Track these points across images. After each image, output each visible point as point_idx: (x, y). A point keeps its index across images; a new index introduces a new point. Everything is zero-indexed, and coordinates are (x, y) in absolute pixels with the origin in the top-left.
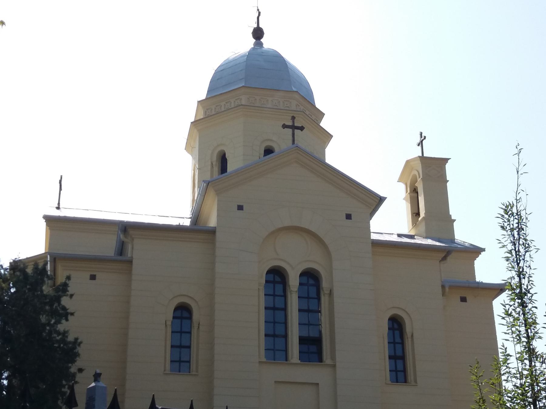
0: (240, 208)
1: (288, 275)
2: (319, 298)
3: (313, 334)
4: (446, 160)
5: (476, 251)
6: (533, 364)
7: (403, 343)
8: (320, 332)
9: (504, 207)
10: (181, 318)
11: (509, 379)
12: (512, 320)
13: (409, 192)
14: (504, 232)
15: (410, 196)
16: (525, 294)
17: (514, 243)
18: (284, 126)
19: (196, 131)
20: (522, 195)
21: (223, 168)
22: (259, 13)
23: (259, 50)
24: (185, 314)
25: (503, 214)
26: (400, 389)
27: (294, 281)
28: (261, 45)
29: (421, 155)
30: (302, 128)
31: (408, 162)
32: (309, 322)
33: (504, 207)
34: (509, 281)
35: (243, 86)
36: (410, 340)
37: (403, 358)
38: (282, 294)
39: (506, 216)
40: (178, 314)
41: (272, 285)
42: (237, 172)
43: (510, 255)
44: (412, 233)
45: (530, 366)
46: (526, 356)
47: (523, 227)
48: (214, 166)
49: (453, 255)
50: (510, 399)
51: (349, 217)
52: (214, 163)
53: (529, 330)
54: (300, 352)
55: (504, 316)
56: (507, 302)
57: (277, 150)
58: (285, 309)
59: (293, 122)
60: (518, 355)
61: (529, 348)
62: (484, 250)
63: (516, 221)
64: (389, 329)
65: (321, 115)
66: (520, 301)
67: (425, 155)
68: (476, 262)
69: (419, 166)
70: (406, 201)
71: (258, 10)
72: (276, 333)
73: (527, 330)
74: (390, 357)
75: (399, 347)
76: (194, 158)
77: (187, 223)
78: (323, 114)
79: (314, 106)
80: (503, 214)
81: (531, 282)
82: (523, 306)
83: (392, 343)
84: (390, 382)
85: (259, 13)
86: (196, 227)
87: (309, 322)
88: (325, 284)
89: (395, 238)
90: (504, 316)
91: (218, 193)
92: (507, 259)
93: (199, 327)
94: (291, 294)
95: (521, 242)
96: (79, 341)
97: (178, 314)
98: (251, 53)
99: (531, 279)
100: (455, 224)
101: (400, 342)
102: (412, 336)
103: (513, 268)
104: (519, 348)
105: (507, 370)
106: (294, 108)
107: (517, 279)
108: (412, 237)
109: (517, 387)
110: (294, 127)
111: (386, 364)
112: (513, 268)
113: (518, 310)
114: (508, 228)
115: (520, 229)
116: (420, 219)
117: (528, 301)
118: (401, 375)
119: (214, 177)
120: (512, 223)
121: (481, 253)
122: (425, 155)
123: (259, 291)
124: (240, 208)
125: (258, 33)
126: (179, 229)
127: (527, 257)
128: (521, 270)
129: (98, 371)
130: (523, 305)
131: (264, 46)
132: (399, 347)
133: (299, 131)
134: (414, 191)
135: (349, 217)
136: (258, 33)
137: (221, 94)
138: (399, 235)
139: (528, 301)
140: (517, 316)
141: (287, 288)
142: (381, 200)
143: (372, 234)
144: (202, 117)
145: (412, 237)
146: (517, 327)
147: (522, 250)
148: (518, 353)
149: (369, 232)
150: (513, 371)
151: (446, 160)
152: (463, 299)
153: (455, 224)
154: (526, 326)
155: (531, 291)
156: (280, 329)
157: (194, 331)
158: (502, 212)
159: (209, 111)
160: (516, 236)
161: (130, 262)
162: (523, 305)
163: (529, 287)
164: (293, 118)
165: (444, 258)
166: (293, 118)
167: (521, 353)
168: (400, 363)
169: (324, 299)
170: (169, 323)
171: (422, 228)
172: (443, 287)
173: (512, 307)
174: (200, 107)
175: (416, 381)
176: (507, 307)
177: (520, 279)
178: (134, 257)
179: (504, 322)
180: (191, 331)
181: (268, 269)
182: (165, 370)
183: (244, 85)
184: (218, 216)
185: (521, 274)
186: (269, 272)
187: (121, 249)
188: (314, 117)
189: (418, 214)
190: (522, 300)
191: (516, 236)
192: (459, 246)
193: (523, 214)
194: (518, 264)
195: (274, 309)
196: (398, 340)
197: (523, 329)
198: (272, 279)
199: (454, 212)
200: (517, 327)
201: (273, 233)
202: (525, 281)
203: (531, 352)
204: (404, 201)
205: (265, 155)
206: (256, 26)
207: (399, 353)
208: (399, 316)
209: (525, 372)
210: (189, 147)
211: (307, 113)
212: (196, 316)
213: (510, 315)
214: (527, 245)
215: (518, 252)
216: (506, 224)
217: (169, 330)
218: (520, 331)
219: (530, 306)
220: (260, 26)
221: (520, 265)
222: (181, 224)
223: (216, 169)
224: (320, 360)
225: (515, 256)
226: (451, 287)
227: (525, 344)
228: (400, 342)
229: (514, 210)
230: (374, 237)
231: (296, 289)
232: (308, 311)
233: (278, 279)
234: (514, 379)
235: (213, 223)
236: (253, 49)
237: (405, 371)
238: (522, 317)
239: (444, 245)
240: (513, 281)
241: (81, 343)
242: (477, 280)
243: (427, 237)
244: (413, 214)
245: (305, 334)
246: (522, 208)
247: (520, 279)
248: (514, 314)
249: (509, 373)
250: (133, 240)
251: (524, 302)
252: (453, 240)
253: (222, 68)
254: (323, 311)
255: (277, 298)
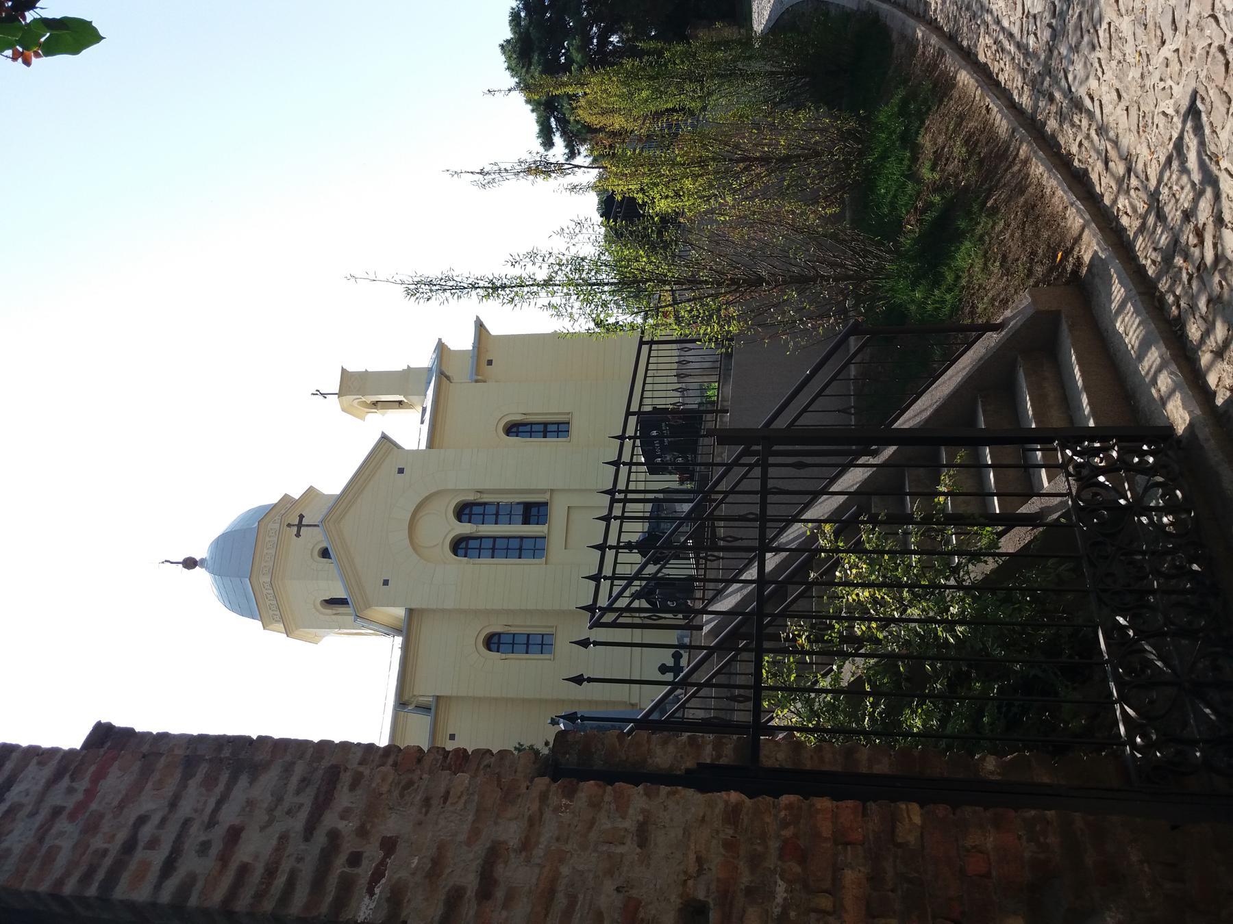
0: (386, 583)
1: (460, 534)
2: (485, 504)
3: (520, 510)
4: (343, 371)
5: (441, 348)
6: (557, 282)
7: (532, 424)
8: (518, 503)
9: (409, 296)
10: (499, 643)
11: (570, 305)
12: (517, 298)
13: (376, 410)
14: (434, 298)
15: (381, 409)
16: (493, 284)
17: (444, 290)
18: (298, 535)
19: (297, 632)
20: (397, 278)
21: (342, 602)
22: (166, 561)
23: (209, 563)
24: (495, 639)
25: (415, 297)
26: (575, 429)
27: (466, 528)
28: (203, 561)
29: (337, 396)
30: (301, 517)
31: (343, 410)
32: (508, 514)
33: (409, 296)
34: (480, 297)
35: (249, 580)
36: (528, 417)
37: (546, 424)
38: (479, 540)
39: (418, 295)
40: (494, 647)
41: (469, 551)
42: (347, 588)
43: (456, 294)
44: (420, 409)
45: (560, 285)
46: (551, 288)
47: (428, 280)
48: (338, 612)
49: (444, 369)
50: (589, 305)
51: (401, 471)
52: (334, 612)
53: (527, 283)
54: (538, 524)
55: (513, 304)
56: (501, 301)
57: (325, 545)
58: (495, 538)
59: (293, 525)
60: (550, 295)
61: (543, 285)
62: (440, 340)
63: (423, 286)
64: (517, 436)
65: (286, 498)
66: (500, 289)
67: (337, 392)
68: (452, 349)
69: (349, 399)
70: (386, 413)
71: (163, 562)
72: (518, 547)
73: (527, 286)
74: (545, 437)
75: (535, 428)
76: (328, 634)
77: (399, 640)
78: (286, 495)
79: (276, 505)
80: (415, 297)
81: (482, 278)
82: (505, 287)
83: (531, 434)
84: (569, 438)
85: (166, 561)
86: (404, 632)
87: (508, 514)
88: (471, 497)
89: (425, 428)
90: (513, 304)
91: (368, 606)
92: (459, 297)
93: (509, 626)
94: (479, 531)
95: (444, 284)
96: (517, 746)
97: (494, 647)
98: (213, 572)
99: (479, 278)
100: (412, 366)
101: (530, 426)
102: (524, 414)
103: (468, 292)
104: (543, 293)
105: (563, 306)
106: (277, 526)
107: (478, 290)
108: (424, 410)
109: (578, 298)
110: (300, 525)
111: (551, 441)
112: (468, 292)
113: (508, 292)
114: (430, 294)
115: (430, 283)
116: (406, 401)
117: (500, 282)
118: (562, 427)
119: (352, 612)
120: (424, 290)
121: (535, 114)
122: (337, 392)
123: (475, 564)
124: (386, 583)
125: (190, 563)
126: (406, 649)
127: (459, 279)
128: (471, 286)
129: (549, 721)
130: (504, 287)
131: (204, 557)
132: (535, 428)
133: (304, 519)
134: (375, 404)
135: (401, 471)
136: (190, 563)
137: (257, 604)
138: (422, 422)
139: (500, 282)
140: (513, 293)
141: (474, 535)
142: (384, 437)
143: (420, 448)
144: (282, 625)
145: (424, 410)
146: (524, 293)
147: (451, 283)
148: (547, 295)
149: (418, 451)
150: (564, 301)
151: (343, 371)
152: (490, 363)
153: (412, 366)
154: (523, 286)
155: (491, 278)
156: (515, 544)
157: (513, 630)
158: (413, 298)
159: (275, 617)
160: (437, 287)
161: (438, 698)
162: (504, 287)
163: (487, 280)
164: (289, 525)
165: (448, 378)
166: (289, 525)
167: (548, 292)
168: (550, 428)
169: (486, 498)
170: (504, 656)
171: (414, 399)
172: (477, 381)
173: (506, 297)
174: (271, 627)
175: (568, 413)
176: (504, 301)
177: (479, 287)
178: (433, 694)
179: (519, 305)
180: (511, 634)
181: (453, 555)
182: (550, 660)
183: (248, 579)
184: (394, 606)
185: (474, 287)
186: (456, 554)
187: (424, 709)
188: (289, 505)
189: (400, 402)
190: (499, 287)
191: (437, 287)
192: (436, 363)
193: (416, 279)
194: (465, 288)
195: (493, 549)
196: (528, 428)
197: (526, 289)
198: (463, 551)
199: (399, 366)
200: (524, 293)
201: (414, 549)
202: (481, 284)
203: (547, 283)
204: (386, 415)
205: (330, 558)
206: (181, 566)
207: (541, 428)
208: (504, 426)
209: (565, 290)
210: (314, 640)
211: (283, 512)
212: (498, 629)
213: (513, 299)
214: (447, 278)
215: (452, 288)
216: (426, 296)
217: (511, 656)
218: (528, 292)
219: (505, 281)
220: (181, 561)
221: (466, 286)
222: (400, 646)
223: (342, 609)
224: (546, 504)
225: (456, 290)
226: (477, 374)
227: (539, 288)
228: (530, 426)
229: (412, 287)
230: (423, 446)
231: (475, 526)
232: (497, 514)
233: (463, 545)
234: (571, 301)
235: (400, 612)
236: (207, 568)
237: (558, 424)
238: (515, 289)
239: (434, 378)
240: (481, 294)
241: (519, 744)
242: (471, 348)
243: (425, 395)
244: (400, 408)
245: (520, 518)
246: (410, 280)
247: (479, 287)
248: (512, 295)
249: (565, 305)
250: (415, 696)
251: (501, 285)
252: (430, 370)
253: (228, 604)
254: (498, 500)
255: (482, 547)
